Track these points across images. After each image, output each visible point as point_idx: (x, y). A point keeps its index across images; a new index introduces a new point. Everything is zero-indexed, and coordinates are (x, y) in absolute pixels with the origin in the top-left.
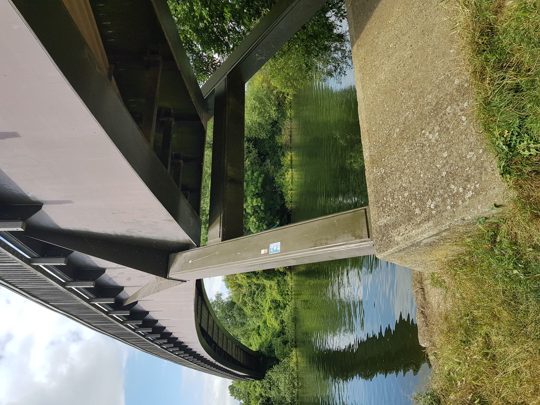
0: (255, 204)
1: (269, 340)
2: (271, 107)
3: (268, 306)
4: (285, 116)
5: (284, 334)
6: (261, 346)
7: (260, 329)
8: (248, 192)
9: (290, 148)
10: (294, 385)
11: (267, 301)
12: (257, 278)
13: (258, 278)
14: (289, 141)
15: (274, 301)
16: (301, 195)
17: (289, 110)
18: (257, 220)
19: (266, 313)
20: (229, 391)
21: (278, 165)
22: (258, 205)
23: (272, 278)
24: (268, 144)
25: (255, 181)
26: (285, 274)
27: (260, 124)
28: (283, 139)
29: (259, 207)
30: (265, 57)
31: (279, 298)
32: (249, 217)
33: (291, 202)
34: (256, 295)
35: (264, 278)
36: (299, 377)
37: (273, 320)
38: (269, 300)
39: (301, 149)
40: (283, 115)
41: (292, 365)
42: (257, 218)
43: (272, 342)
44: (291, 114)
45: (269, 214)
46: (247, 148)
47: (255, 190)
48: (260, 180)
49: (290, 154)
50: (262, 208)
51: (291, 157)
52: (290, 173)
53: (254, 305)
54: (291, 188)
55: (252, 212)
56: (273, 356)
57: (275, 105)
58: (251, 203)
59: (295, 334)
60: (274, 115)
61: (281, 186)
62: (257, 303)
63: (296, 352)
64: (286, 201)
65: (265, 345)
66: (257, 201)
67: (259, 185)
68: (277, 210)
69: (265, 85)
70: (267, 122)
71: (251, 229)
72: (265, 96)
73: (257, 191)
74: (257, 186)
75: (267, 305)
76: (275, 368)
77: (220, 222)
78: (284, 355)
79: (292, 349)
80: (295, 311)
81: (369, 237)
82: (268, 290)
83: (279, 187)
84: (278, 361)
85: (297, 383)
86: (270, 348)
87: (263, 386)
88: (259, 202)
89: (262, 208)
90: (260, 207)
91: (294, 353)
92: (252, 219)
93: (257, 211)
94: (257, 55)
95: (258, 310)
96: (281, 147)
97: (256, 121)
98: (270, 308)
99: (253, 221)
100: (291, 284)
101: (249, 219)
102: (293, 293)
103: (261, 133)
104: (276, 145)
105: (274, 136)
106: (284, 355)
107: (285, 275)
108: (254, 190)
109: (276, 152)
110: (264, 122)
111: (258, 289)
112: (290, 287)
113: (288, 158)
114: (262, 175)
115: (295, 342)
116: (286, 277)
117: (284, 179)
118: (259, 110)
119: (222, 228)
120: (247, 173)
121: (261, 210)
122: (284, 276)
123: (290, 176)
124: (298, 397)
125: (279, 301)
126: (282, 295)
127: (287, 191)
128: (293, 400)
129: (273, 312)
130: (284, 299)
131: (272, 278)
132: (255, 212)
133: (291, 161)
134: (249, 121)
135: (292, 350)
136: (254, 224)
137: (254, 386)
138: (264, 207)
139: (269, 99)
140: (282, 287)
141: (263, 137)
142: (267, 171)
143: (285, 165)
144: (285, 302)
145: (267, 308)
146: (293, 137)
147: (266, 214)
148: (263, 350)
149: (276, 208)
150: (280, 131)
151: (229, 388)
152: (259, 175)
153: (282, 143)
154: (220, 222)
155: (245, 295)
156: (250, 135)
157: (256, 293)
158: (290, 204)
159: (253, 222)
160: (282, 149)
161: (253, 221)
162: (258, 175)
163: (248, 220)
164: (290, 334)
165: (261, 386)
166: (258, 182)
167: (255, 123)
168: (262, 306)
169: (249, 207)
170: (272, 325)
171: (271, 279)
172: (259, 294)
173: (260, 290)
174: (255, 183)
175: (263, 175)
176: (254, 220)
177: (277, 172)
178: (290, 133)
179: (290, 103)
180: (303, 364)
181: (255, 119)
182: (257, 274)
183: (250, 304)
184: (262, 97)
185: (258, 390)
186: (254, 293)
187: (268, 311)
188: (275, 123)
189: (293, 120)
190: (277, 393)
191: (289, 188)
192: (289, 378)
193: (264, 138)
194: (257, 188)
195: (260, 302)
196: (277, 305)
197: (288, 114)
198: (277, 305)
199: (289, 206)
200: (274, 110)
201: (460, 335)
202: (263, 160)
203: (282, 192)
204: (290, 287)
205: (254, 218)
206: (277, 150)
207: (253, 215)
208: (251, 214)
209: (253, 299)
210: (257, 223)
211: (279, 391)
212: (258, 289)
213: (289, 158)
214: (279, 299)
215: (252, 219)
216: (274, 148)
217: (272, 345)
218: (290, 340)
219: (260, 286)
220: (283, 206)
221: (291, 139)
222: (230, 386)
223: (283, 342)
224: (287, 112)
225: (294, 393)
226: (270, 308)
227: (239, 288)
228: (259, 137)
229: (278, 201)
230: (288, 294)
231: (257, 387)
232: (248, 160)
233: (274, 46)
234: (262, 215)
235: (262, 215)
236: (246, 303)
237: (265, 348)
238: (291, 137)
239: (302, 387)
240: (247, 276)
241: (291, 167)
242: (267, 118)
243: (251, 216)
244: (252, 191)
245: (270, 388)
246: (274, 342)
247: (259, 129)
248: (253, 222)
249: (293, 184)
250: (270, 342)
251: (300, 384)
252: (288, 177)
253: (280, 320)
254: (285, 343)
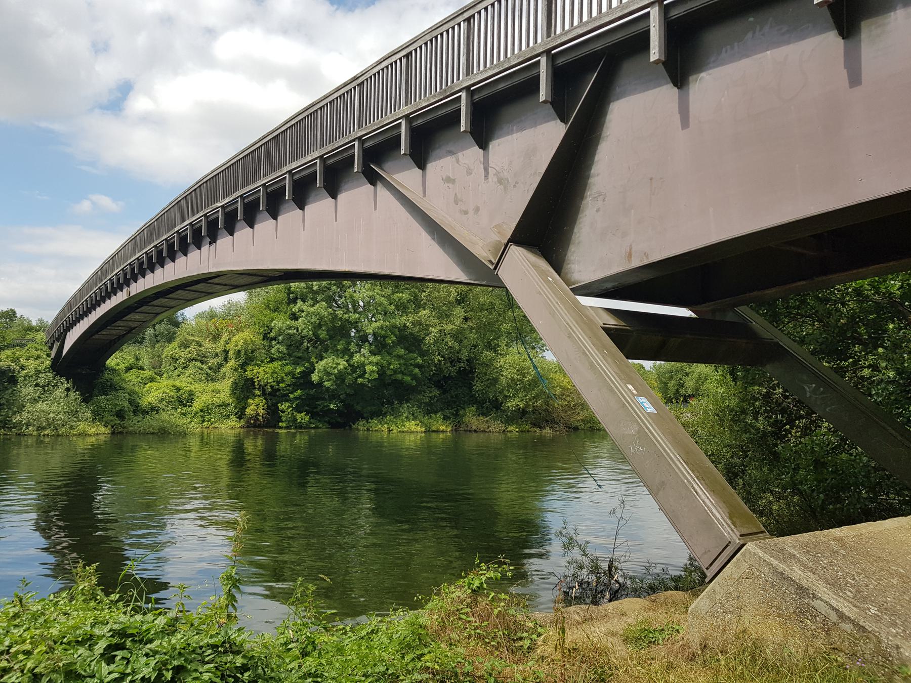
0: (368, 368)
1: (124, 385)
2: (523, 400)
3: (183, 385)
4: (508, 423)
5: (135, 412)
6: (113, 371)
7: (139, 371)
8: (388, 358)
9: (456, 430)
10: (44, 428)
11: (191, 384)
12: (235, 367)
13: (236, 370)
14: (469, 428)
15: (191, 397)
16: (379, 444)
17: (517, 430)
18: (340, 372)
19: (171, 382)
20: (5, 309)
21: (430, 409)
22: (366, 373)
23: (235, 393)
24: (463, 394)
25: (405, 369)
26: (240, 418)
27: (496, 380)
28: (472, 419)
29: (362, 376)
30: (810, 396)
31: (197, 405)
32: (346, 358)
33: (368, 430)
34: (200, 364)
35: (235, 380)
36: (60, 438)
37: (160, 394)
38: (192, 387)
39: (455, 447)
40: (509, 420)
41: (82, 426)
42: (344, 370)
43: (121, 391)
44: (511, 431)
45: (348, 391)
46: (458, 358)
47: (392, 369)
48: (407, 379)
49: (448, 430)
50: (360, 380)
51: (443, 431)
52: (419, 429)
53: (183, 361)
54: (392, 430)
55: (354, 363)
56: (96, 391)
57: (527, 405)
58: (370, 363)
59: (136, 433)
60: (512, 404)
61: (396, 414)
62: (185, 367)
63: (104, 434)
64: (370, 420)
65: (116, 379)
66: (373, 371)
67: (399, 377)
68: (353, 405)
69: (558, 391)
70: (499, 392)
71: (326, 360)
72: (541, 390)
73: (389, 372)
74: (398, 374)
75: (185, 382)
76: (74, 395)
77: (620, 325)
78: (98, 411)
79: (109, 427)
80: (180, 433)
81: (741, 535)
82: (211, 386)
83: (393, 409)
84: (86, 400)
85: (48, 435)
86: (111, 386)
87: (40, 372)
88: (371, 375)
89: (360, 380)
90: (362, 376)
91: (103, 429)
92: (342, 363)
93: (355, 372)
94: (814, 385)
95: (172, 368)
96: (456, 415)
97: (502, 376)
98: (178, 389)
99: (339, 364)
100: (223, 427)
101: (341, 358)
102: (205, 431)
103: (482, 383)
104: (460, 406)
105: (474, 404)
106: (98, 411)
107: (238, 418)
108: (392, 367)
109: (448, 405)
110: (499, 388)
111: (210, 368)
112: (216, 425)
113: (444, 428)
114: (414, 381)
115: (121, 433)
116: (233, 418)
117: (407, 418)
118: (518, 380)
119: (614, 328)
120: (419, 358)
121: (357, 378)
122: (236, 414)
123: (413, 428)
124: (19, 434)
125: (191, 406)
126: (202, 410)
127: (386, 423)
128: (18, 425)
129: (173, 394)
130: (195, 414)
131: (235, 393)
132: (354, 368)
133: (437, 431)
134: (502, 363)
135: (107, 427)
136: (334, 366)
137: (38, 357)
138: (362, 384)
139: (536, 398)
140: (217, 411)
141: (475, 385)
142: (420, 391)
143: (430, 420)
144: (189, 416)
145: (178, 384)
146: (474, 435)
147: (350, 386)
148: (107, 375)
149: (358, 403)
150: (484, 414)
151: (11, 310)
152: (414, 377)
153: (464, 415)
154: (620, 325)
155: (200, 346)
156: (479, 364)
157: (203, 366)
158: (365, 428)
159: (338, 364)
160: (454, 415)
161: (339, 364)
162: (416, 374)
163: (340, 355)
164: (135, 423)
165: (40, 368)
166: (403, 375)
167: (497, 372)
168: (179, 376)
169: (363, 359)
170: (149, 392)
171: (233, 393)
172: (202, 370)
173: (209, 371)
174: (403, 370)
175: (414, 383)
176: (342, 367)
177: (419, 407)
178: (482, 429)
179: (528, 431)
180: (82, 445)
181: (504, 374)
182: (241, 368)
183: (183, 354)
184: (539, 386)
185: (32, 364)
186: (202, 363)
187: (174, 386)
188: (496, 405)
189: (502, 436)
190: (29, 397)
191: (393, 427)
192: (57, 420)
193: (474, 387)
194: (395, 372)
195: (187, 372)
196: (184, 402)
197: (512, 428)
198: (184, 402)
199: (361, 425)
200: (518, 405)
202: (438, 385)
203: (385, 415)
204: (216, 425)
205: (344, 365)
206: (452, 408)
207: (349, 365)
208: (351, 362)
209: (192, 360)
210: (336, 371)
211: (35, 401)
212: (210, 368)
213: (442, 428)
214: (195, 404)
215: (342, 363)
216: (455, 402)
217: (117, 390)
218: (126, 423)
219: (216, 373)
220: (359, 416)
221: (470, 431)
222: (15, 312)
223: (121, 410)
224: (515, 426)
225: (28, 428)
226: (180, 390)
227: (211, 337)
228: (476, 379)
229: (369, 408)
230: (204, 421)
231: (38, 362)
232: (440, 359)
233: (829, 410)
234: (349, 380)
235: (349, 380)
236: (186, 347)
237: (111, 379)
238: (476, 431)
239: (39, 442)
240: (239, 351)
241: (428, 431)
242: (506, 393)
243: (347, 361)
244: (390, 364)
245: (37, 385)
246: (121, 393)
247: (488, 380)
248: (338, 364)
249: (399, 434)
250: (120, 387)
251: (46, 440)
252: (412, 425)
253: (158, 407)
254: (120, 415)
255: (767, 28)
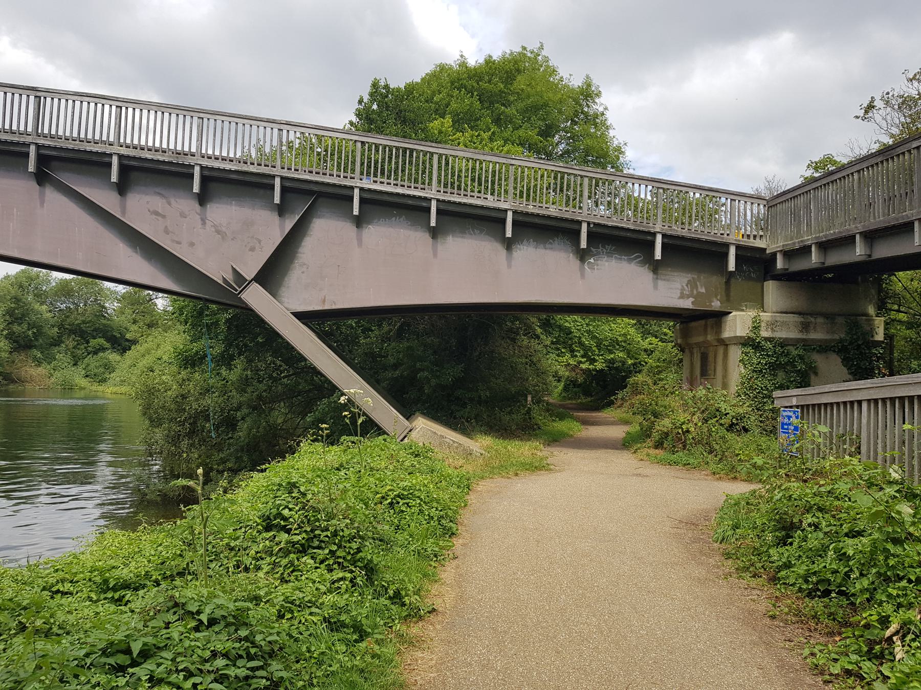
201: (171, 604)
255: (401, 219)
